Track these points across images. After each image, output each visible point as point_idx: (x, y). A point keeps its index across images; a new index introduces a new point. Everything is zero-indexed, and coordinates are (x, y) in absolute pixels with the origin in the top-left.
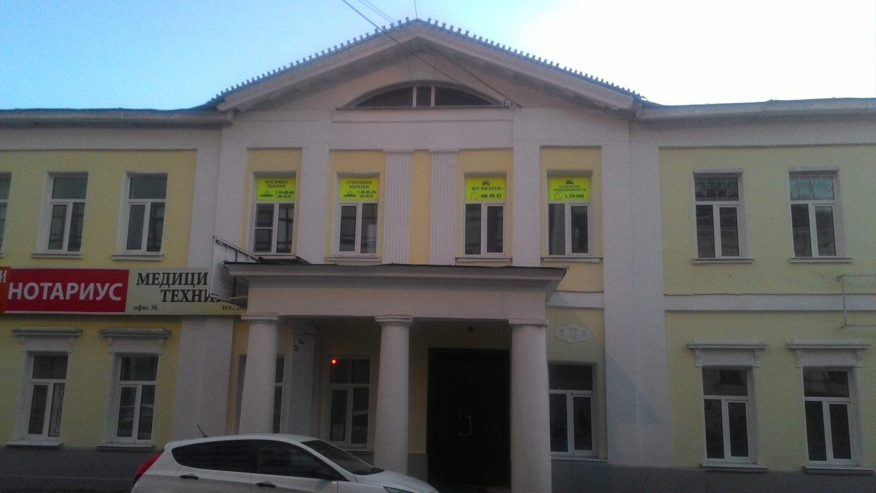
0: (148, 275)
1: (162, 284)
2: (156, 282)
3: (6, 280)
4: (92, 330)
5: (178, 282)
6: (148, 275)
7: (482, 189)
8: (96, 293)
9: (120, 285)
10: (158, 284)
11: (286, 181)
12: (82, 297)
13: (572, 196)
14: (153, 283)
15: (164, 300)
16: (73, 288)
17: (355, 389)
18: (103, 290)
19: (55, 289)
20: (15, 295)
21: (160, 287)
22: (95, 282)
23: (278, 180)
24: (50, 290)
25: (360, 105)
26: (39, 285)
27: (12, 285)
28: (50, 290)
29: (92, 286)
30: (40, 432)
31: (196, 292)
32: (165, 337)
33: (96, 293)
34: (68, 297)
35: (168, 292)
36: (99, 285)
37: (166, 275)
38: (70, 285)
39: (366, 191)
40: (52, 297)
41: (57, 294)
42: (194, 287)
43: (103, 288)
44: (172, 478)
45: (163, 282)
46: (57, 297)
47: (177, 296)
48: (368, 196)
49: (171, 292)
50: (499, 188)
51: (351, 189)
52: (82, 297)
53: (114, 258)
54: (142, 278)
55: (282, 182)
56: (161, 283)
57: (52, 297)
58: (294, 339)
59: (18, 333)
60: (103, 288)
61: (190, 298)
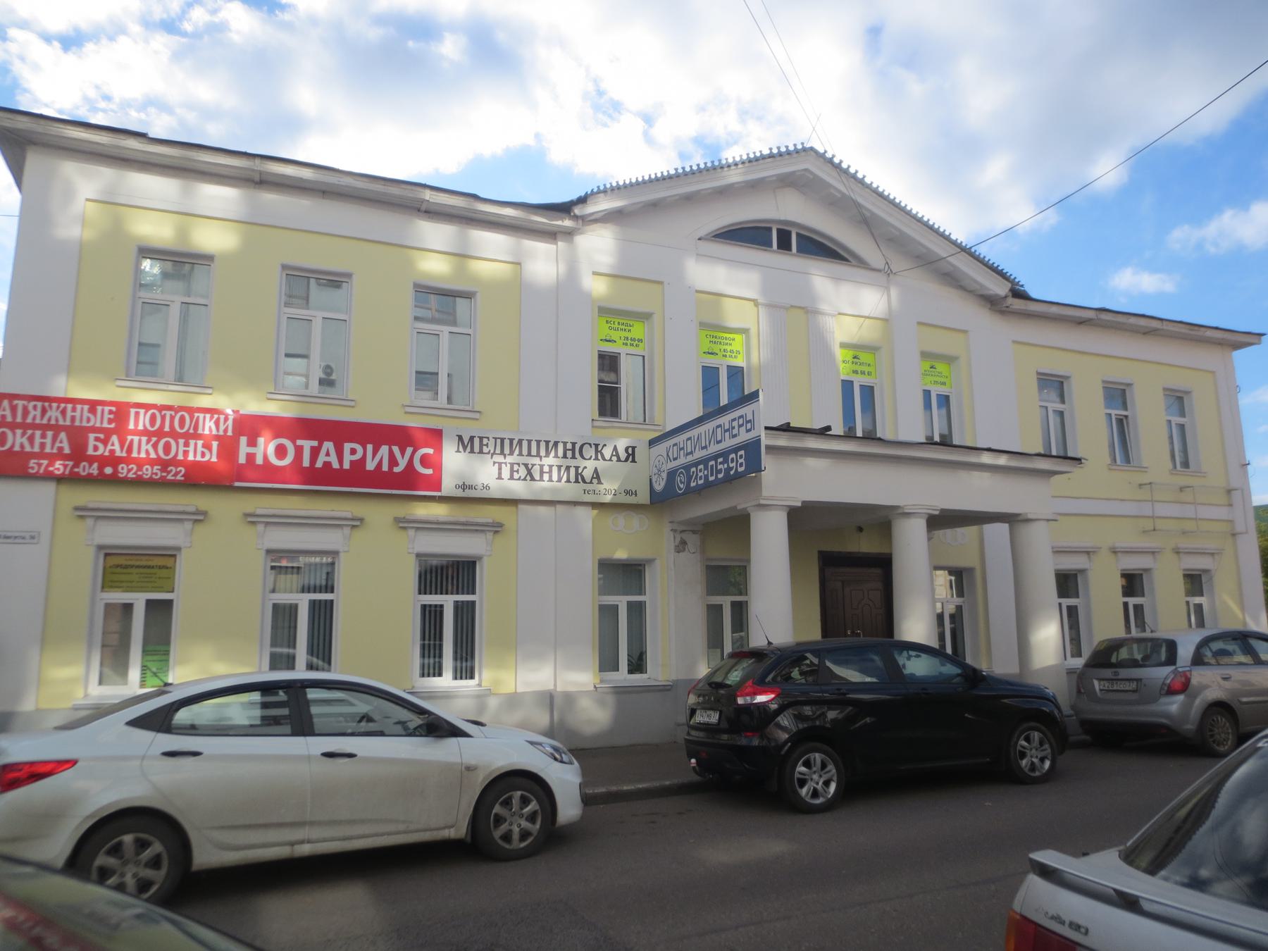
0: (472, 439)
1: (494, 453)
2: (485, 449)
3: (233, 431)
4: (379, 514)
5: (517, 452)
6: (472, 439)
7: (853, 363)
8: (393, 461)
9: (430, 451)
10: (489, 453)
11: (631, 324)
12: (370, 465)
13: (936, 382)
14: (481, 452)
15: (500, 478)
16: (352, 452)
17: (456, 603)
18: (403, 457)
19: (323, 451)
20: (250, 457)
21: (492, 458)
22: (390, 444)
23: (621, 321)
24: (315, 452)
25: (716, 236)
26: (294, 443)
27: (243, 440)
28: (315, 452)
29: (384, 450)
30: (616, 668)
31: (544, 467)
32: (496, 528)
33: (393, 461)
34: (346, 466)
35: (503, 465)
36: (396, 449)
37: (499, 441)
38: (347, 447)
39: (729, 350)
40: (319, 464)
41: (327, 459)
42: (541, 460)
43: (403, 454)
44: (309, 758)
45: (495, 451)
46: (327, 465)
47: (517, 471)
48: (625, 330)
49: (509, 465)
50: (869, 365)
51: (712, 345)
52: (370, 465)
53: (353, 403)
54: (463, 443)
55: (627, 325)
56: (492, 452)
57: (319, 464)
58: (675, 538)
59: (251, 519)
60: (403, 454)
61: (537, 477)
